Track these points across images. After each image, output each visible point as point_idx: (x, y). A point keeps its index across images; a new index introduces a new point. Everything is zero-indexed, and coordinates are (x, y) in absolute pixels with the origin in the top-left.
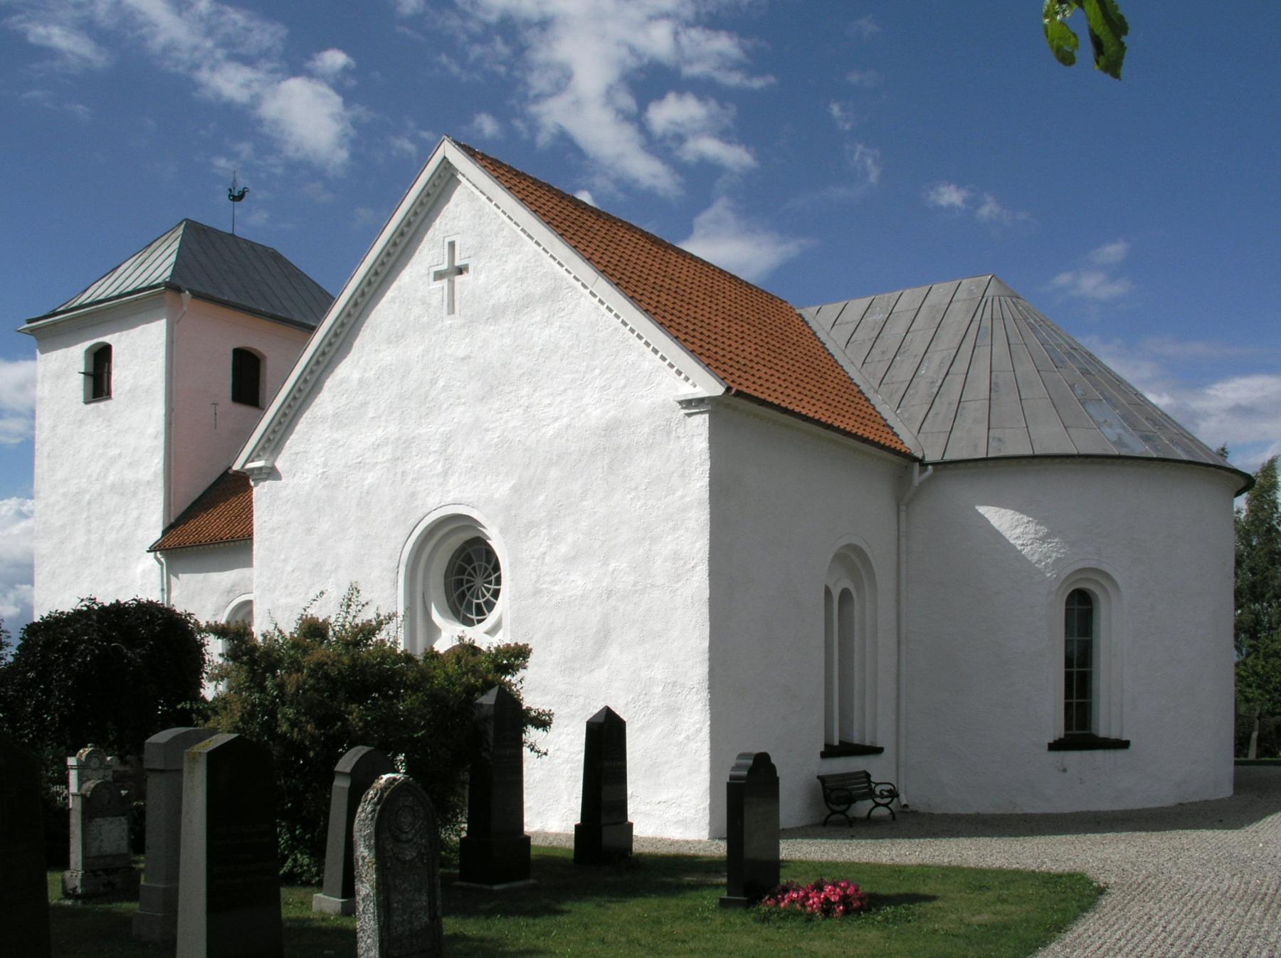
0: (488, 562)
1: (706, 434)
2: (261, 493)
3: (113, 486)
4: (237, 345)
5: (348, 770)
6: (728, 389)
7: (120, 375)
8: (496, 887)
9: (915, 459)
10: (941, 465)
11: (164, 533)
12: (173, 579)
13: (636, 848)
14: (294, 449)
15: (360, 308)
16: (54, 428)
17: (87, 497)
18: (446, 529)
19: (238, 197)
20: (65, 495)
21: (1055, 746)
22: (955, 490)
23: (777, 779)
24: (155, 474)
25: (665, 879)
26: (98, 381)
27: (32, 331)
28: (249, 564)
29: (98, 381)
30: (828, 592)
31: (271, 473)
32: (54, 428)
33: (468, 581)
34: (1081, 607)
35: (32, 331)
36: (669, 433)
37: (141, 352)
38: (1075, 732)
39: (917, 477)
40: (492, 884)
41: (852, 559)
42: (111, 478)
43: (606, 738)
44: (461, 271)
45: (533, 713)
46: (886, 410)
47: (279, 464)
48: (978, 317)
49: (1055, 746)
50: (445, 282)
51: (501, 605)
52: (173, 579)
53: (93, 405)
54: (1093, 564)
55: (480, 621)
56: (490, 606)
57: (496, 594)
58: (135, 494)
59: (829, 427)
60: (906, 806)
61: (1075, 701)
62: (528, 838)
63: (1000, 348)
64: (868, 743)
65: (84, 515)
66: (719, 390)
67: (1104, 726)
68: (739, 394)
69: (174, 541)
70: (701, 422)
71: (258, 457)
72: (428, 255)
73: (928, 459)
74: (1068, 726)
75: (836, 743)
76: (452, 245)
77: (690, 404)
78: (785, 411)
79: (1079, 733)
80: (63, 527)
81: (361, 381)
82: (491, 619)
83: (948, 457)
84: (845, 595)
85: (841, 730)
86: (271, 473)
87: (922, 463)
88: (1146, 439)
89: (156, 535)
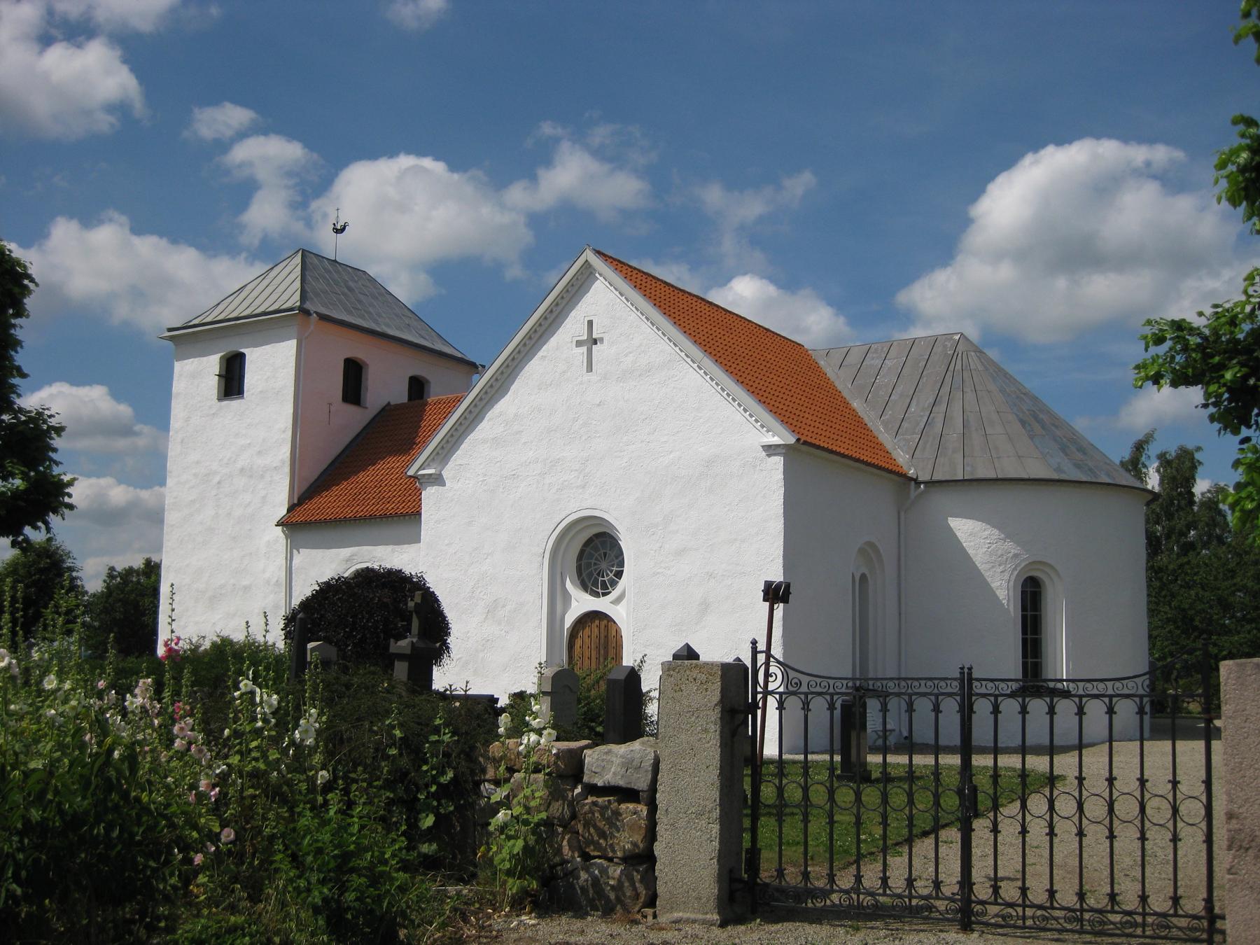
1: (781, 469)
2: (429, 496)
3: (242, 470)
4: (349, 355)
6: (798, 440)
7: (252, 378)
9: (911, 479)
10: (931, 483)
11: (289, 511)
12: (295, 551)
14: (459, 462)
15: (516, 362)
16: (187, 420)
17: (217, 479)
18: (579, 527)
19: (340, 231)
20: (195, 475)
22: (940, 500)
24: (283, 462)
26: (232, 381)
27: (171, 338)
29: (232, 381)
31: (438, 480)
32: (187, 420)
34: (1032, 594)
35: (171, 338)
36: (755, 467)
37: (273, 366)
39: (913, 493)
41: (869, 552)
42: (239, 465)
44: (595, 342)
46: (885, 438)
47: (446, 474)
48: (951, 368)
50: (584, 349)
51: (623, 583)
52: (295, 551)
53: (225, 403)
54: (1039, 559)
55: (604, 594)
56: (614, 584)
57: (619, 574)
58: (262, 477)
59: (858, 460)
63: (970, 396)
65: (214, 492)
66: (791, 440)
68: (805, 443)
69: (296, 518)
70: (778, 461)
71: (429, 466)
72: (573, 326)
73: (920, 479)
76: (590, 323)
77: (770, 450)
78: (831, 452)
80: (193, 502)
81: (516, 415)
82: (615, 594)
83: (935, 478)
86: (438, 480)
87: (917, 482)
88: (1078, 466)
89: (283, 511)
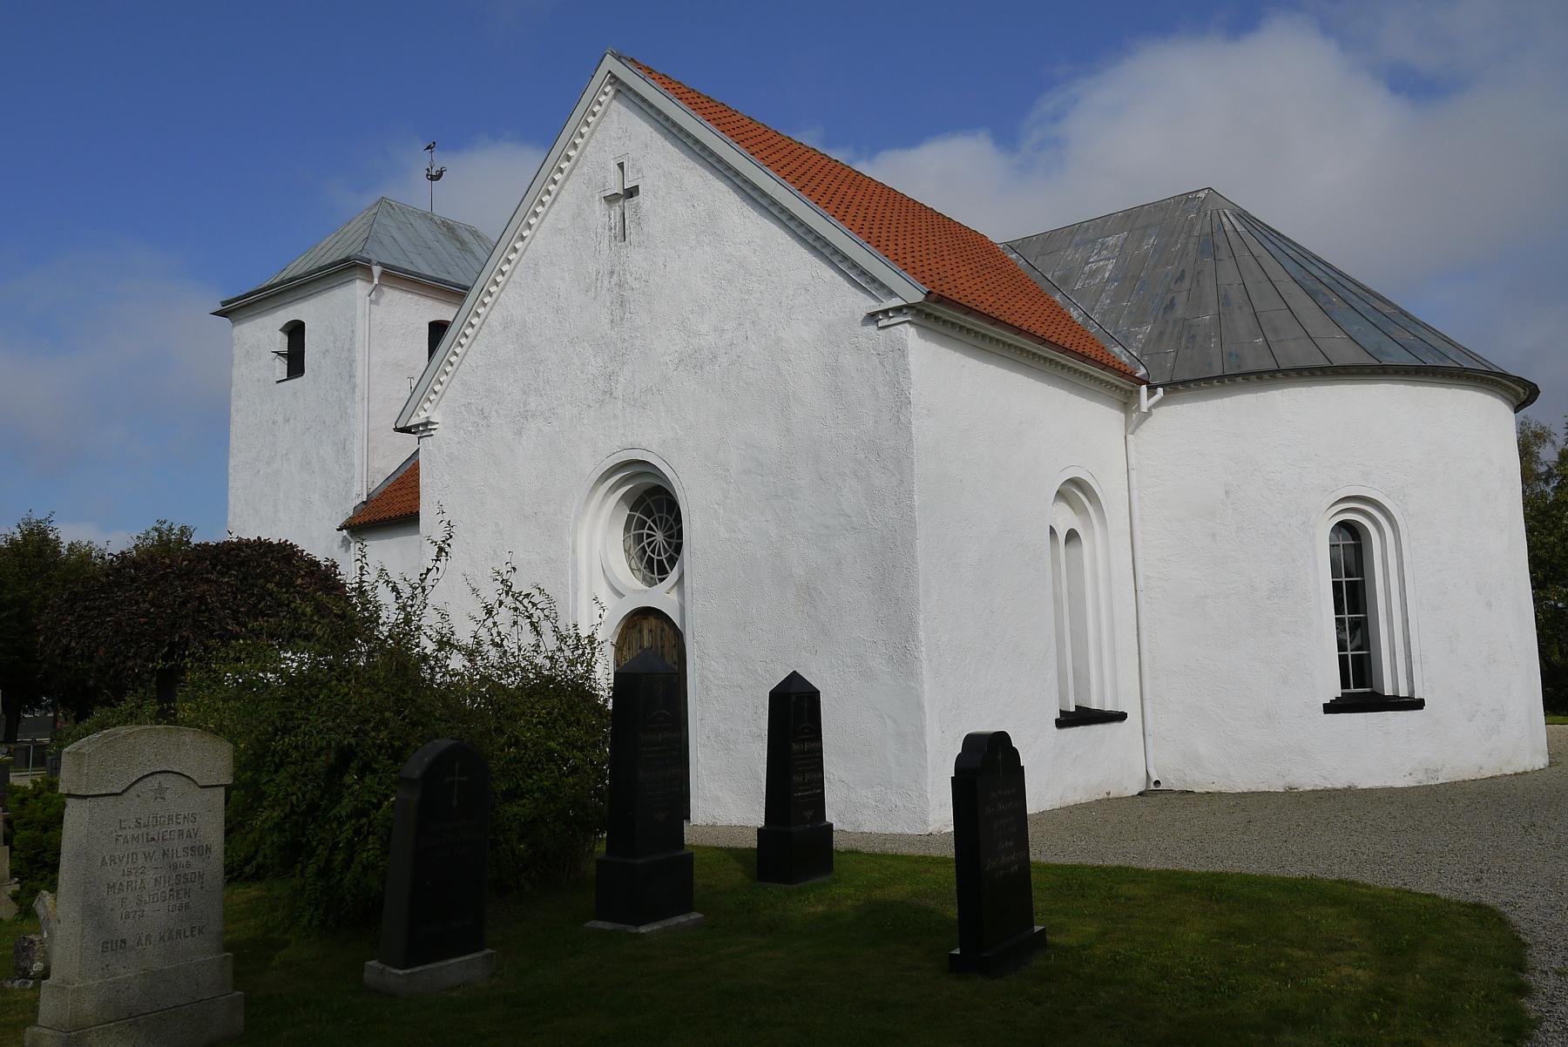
0: (669, 512)
5: (418, 773)
8: (643, 930)
13: (690, 836)
21: (1330, 708)
23: (1153, 792)
25: (1289, 951)
28: (418, 532)
30: (1052, 531)
33: (649, 536)
38: (1353, 690)
40: (638, 925)
43: (794, 714)
45: (19, 537)
49: (1330, 708)
55: (661, 580)
60: (1157, 783)
61: (1350, 653)
62: (690, 856)
64: (1108, 708)
66: (920, 297)
67: (1390, 683)
68: (941, 300)
74: (1345, 683)
75: (1073, 709)
79: (1361, 690)
84: (1072, 535)
85: (1076, 693)
